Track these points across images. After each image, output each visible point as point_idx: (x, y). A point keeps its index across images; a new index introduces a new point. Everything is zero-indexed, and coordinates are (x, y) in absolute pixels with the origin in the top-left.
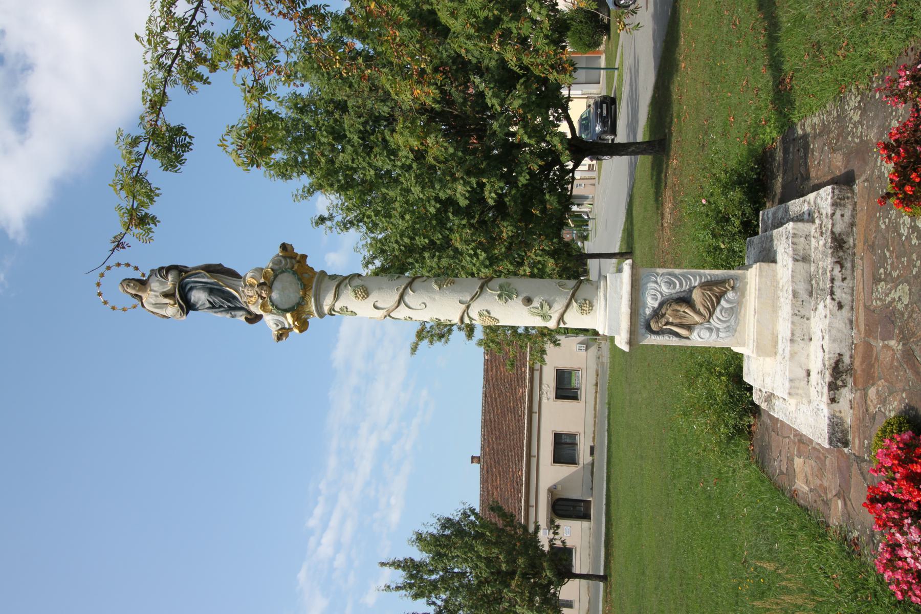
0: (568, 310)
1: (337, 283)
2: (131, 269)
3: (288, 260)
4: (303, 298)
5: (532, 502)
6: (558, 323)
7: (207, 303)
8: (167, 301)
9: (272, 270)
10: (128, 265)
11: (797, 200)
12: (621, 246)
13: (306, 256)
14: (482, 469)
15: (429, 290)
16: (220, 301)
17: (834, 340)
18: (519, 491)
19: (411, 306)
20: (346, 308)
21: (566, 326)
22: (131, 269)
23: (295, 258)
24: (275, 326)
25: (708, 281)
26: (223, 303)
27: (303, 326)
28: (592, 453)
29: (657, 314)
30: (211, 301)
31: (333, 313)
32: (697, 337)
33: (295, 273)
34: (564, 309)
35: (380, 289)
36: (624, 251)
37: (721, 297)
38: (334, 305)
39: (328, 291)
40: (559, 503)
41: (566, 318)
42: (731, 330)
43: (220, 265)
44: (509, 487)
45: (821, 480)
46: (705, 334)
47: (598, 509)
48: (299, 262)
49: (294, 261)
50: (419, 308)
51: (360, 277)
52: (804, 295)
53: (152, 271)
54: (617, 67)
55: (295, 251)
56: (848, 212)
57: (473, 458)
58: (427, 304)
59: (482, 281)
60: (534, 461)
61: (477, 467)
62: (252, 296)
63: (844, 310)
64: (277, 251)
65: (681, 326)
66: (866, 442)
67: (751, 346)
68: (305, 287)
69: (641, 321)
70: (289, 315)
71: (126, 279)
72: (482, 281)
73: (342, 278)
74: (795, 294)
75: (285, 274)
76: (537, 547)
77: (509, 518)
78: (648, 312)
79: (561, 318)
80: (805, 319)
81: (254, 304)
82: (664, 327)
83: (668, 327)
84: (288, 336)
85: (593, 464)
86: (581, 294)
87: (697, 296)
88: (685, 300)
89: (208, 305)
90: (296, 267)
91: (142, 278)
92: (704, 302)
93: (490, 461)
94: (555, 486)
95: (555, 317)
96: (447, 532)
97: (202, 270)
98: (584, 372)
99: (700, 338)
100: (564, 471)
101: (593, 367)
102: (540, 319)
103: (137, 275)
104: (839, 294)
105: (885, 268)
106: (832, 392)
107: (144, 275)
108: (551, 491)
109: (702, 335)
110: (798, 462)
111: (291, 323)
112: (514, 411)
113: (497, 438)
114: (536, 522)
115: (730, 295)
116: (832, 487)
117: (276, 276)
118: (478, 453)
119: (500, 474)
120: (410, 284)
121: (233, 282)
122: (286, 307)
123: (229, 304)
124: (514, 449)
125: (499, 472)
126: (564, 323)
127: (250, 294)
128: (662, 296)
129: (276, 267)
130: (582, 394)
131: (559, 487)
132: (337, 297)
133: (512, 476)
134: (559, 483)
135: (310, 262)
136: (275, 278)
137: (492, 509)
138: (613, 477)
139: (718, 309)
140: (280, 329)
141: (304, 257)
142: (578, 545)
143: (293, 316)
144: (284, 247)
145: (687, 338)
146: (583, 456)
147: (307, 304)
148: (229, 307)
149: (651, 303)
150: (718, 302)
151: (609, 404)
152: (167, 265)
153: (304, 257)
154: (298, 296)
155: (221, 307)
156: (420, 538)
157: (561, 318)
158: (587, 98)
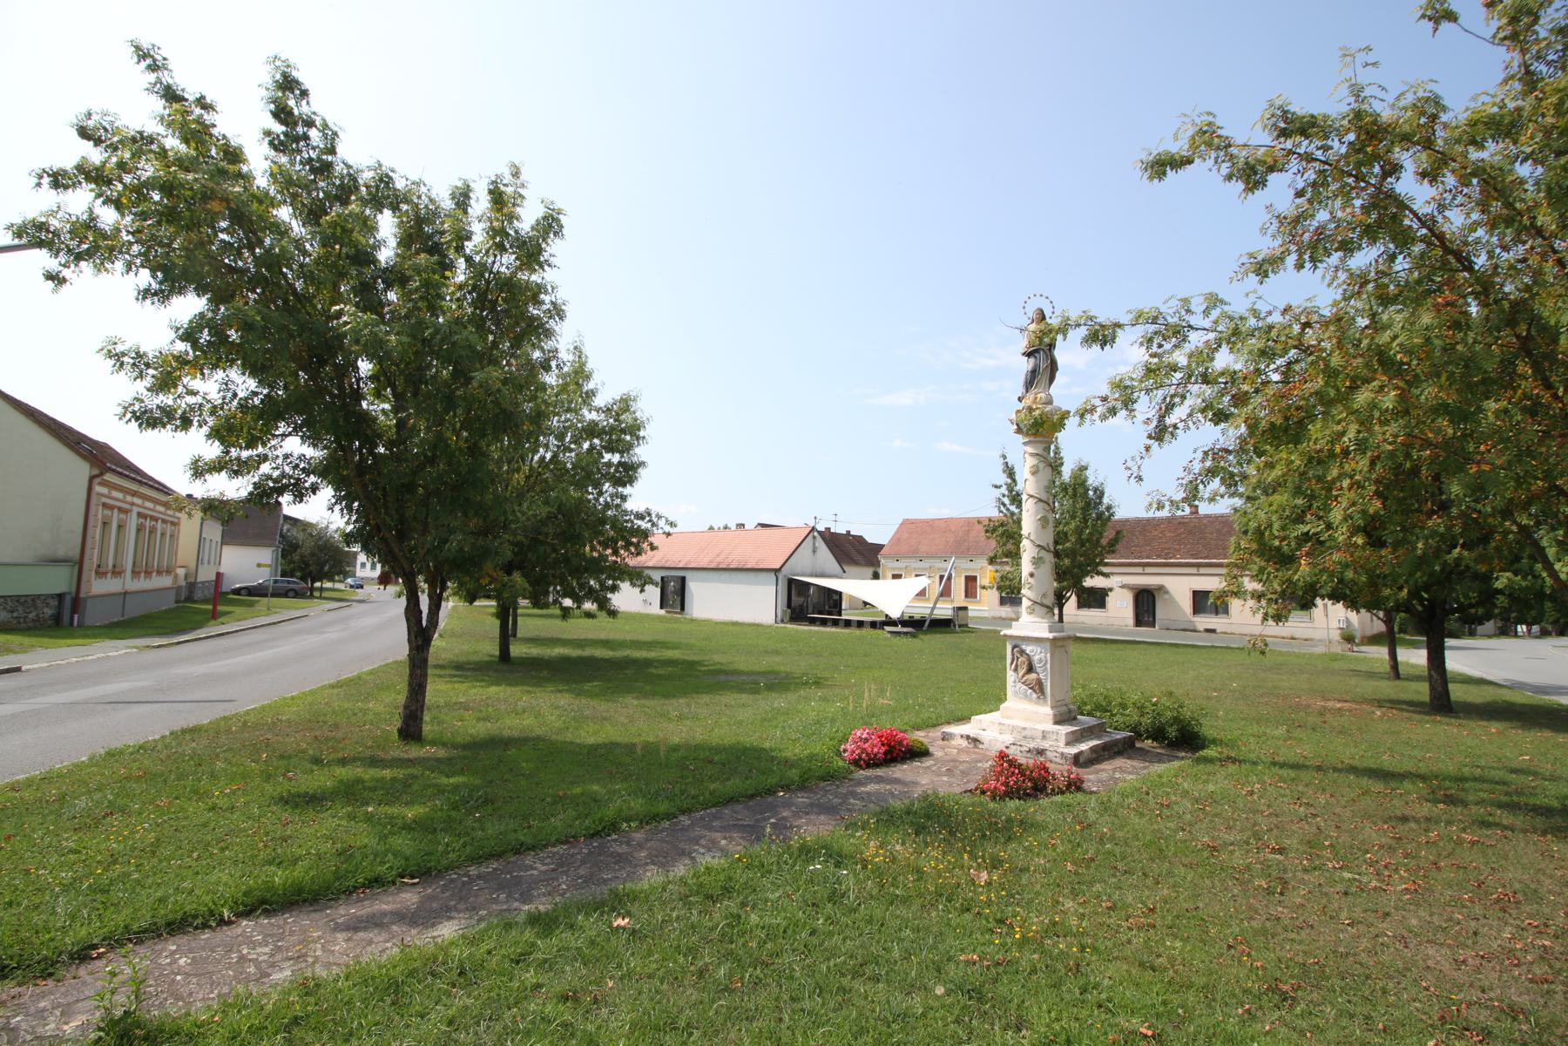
5: (1148, 570)
12: (1407, 664)
15: (1037, 512)
17: (990, 741)
18: (1159, 556)
28: (1208, 631)
29: (1022, 652)
35: (1037, 481)
36: (1400, 668)
39: (1035, 448)
46: (1012, 679)
47: (1145, 634)
52: (1024, 733)
56: (1058, 760)
60: (1194, 570)
65: (1017, 666)
69: (1019, 643)
74: (1024, 729)
76: (1087, 574)
77: (1112, 547)
78: (1024, 647)
85: (1195, 631)
86: (1037, 607)
87: (1033, 676)
88: (1030, 669)
94: (1167, 592)
96: (1091, 493)
98: (1310, 625)
99: (1011, 676)
100: (1186, 604)
101: (1318, 635)
104: (1013, 747)
108: (1161, 588)
113: (1219, 531)
114: (1113, 574)
115: (1035, 696)
120: (1040, 500)
131: (1166, 596)
132: (1032, 455)
134: (1171, 596)
137: (1118, 533)
138: (1113, 646)
142: (1109, 614)
146: (1204, 622)
149: (1028, 649)
151: (1213, 647)
156: (1083, 469)
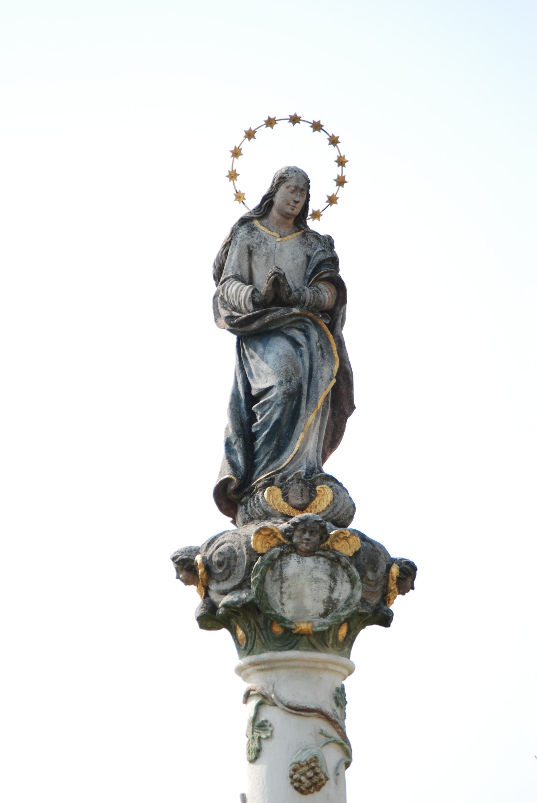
2: (332, 189)
10: (341, 182)
22: (332, 189)
43: (353, 408)
51: (344, 766)
84: (187, 582)
91: (310, 212)
107: (316, 215)
148: (254, 437)
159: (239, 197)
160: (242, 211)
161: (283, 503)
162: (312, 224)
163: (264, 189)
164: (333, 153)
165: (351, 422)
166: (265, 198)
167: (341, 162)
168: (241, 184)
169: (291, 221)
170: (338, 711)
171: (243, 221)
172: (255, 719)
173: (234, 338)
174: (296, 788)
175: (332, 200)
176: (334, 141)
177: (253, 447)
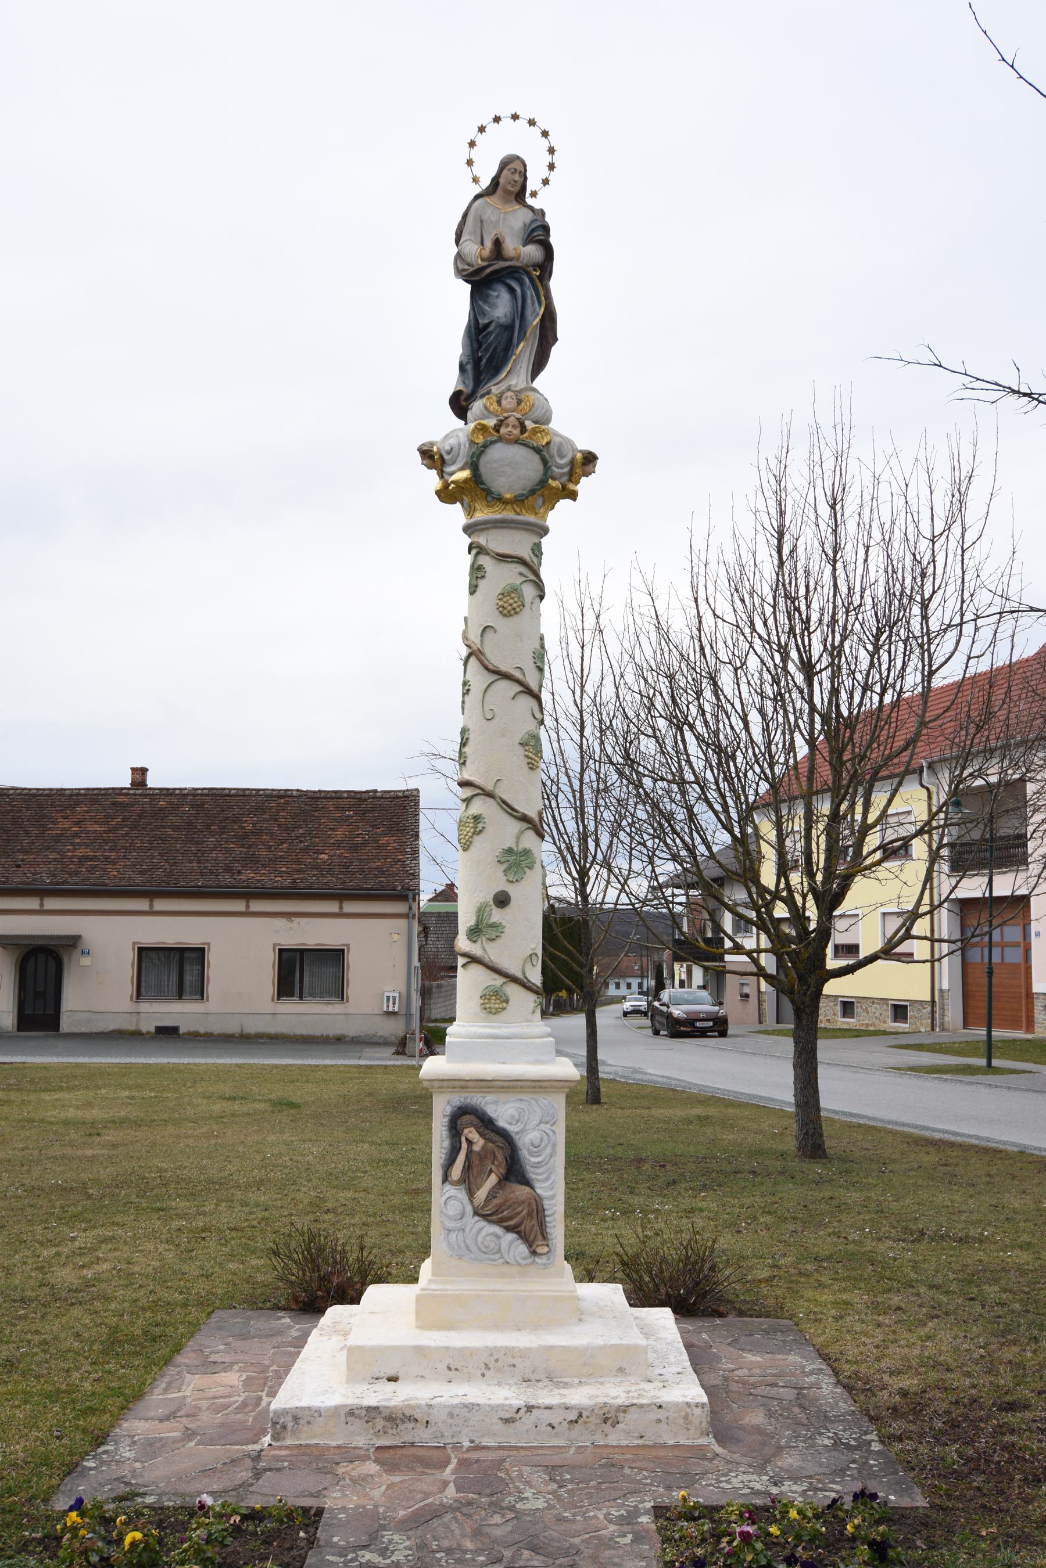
0: (488, 972)
1: (528, 559)
2: (545, 173)
3: (566, 470)
4: (500, 500)
6: (464, 955)
7: (486, 321)
8: (489, 244)
9: (548, 443)
10: (551, 167)
11: (687, 1358)
13: (575, 500)
14: (118, 791)
16: (490, 345)
19: (488, 693)
20: (483, 577)
21: (459, 969)
22: (545, 173)
23: (570, 480)
24: (448, 448)
25: (544, 1210)
26: (486, 350)
27: (446, 495)
30: (491, 328)
31: (474, 552)
32: (447, 1195)
33: (543, 483)
34: (297, 920)
37: (518, 1233)
38: (488, 554)
40: (52, 964)
41: (476, 970)
42: (462, 1252)
43: (556, 339)
44: (81, 852)
45: (208, 1409)
46: (454, 1208)
48: (564, 487)
49: (565, 479)
50: (486, 709)
51: (538, 599)
53: (542, 213)
54: (995, 1063)
55: (583, 479)
57: (144, 771)
58: (494, 721)
59: (537, 819)
61: (125, 781)
62: (499, 403)
63: (500, 1426)
64: (583, 444)
65: (468, 1167)
66: (286, 1464)
67: (433, 1286)
68: (520, 501)
69: (477, 1099)
70: (465, 474)
71: (525, 166)
72: (537, 819)
73: (535, 568)
75: (541, 467)
79: (473, 959)
80: (483, 1371)
81: (486, 407)
82: (463, 1139)
83: (464, 1145)
84: (429, 468)
89: (483, 321)
90: (554, 483)
91: (528, 192)
92: (508, 1204)
93: (137, 809)
95: (475, 949)
97: (546, 309)
102: (472, 922)
103: (533, 183)
105: (571, 1481)
106: (364, 1412)
107: (534, 194)
109: (452, 1202)
110: (234, 1378)
111: (454, 478)
112: (251, 861)
116: (199, 1423)
117: (537, 450)
118: (153, 781)
119: (110, 831)
121: (524, 365)
122: (483, 469)
123: (484, 361)
124: (166, 861)
125: (114, 829)
126: (464, 966)
127: (504, 402)
128: (517, 1133)
129: (554, 449)
130: (290, 1007)
131: (85, 961)
133: (107, 858)
135: (563, 504)
136: (534, 449)
139: (496, 1229)
140: (441, 456)
141: (573, 496)
143: (466, 481)
144: (590, 459)
145: (445, 1179)
147: (489, 506)
148: (480, 359)
150: (508, 1229)
152: (553, 240)
153: (573, 496)
154: (502, 491)
155: (480, 345)
157: (473, 959)
158: (933, 1001)
159: (476, 180)
160: (477, 190)
161: (497, 408)
162: (529, 201)
163: (493, 172)
164: (544, 144)
165: (555, 350)
166: (493, 179)
167: (551, 151)
168: (477, 169)
169: (513, 197)
170: (535, 560)
171: (477, 197)
172: (472, 566)
173: (469, 287)
174: (501, 612)
175: (546, 182)
176: (545, 134)
177: (479, 367)
